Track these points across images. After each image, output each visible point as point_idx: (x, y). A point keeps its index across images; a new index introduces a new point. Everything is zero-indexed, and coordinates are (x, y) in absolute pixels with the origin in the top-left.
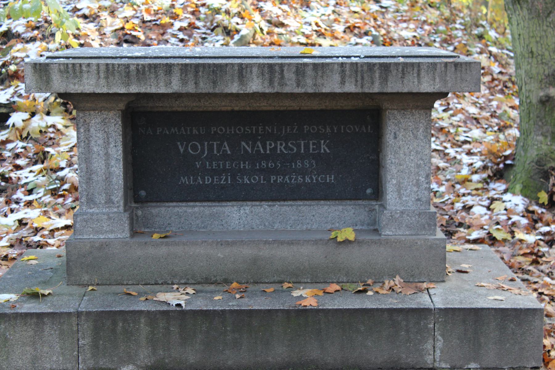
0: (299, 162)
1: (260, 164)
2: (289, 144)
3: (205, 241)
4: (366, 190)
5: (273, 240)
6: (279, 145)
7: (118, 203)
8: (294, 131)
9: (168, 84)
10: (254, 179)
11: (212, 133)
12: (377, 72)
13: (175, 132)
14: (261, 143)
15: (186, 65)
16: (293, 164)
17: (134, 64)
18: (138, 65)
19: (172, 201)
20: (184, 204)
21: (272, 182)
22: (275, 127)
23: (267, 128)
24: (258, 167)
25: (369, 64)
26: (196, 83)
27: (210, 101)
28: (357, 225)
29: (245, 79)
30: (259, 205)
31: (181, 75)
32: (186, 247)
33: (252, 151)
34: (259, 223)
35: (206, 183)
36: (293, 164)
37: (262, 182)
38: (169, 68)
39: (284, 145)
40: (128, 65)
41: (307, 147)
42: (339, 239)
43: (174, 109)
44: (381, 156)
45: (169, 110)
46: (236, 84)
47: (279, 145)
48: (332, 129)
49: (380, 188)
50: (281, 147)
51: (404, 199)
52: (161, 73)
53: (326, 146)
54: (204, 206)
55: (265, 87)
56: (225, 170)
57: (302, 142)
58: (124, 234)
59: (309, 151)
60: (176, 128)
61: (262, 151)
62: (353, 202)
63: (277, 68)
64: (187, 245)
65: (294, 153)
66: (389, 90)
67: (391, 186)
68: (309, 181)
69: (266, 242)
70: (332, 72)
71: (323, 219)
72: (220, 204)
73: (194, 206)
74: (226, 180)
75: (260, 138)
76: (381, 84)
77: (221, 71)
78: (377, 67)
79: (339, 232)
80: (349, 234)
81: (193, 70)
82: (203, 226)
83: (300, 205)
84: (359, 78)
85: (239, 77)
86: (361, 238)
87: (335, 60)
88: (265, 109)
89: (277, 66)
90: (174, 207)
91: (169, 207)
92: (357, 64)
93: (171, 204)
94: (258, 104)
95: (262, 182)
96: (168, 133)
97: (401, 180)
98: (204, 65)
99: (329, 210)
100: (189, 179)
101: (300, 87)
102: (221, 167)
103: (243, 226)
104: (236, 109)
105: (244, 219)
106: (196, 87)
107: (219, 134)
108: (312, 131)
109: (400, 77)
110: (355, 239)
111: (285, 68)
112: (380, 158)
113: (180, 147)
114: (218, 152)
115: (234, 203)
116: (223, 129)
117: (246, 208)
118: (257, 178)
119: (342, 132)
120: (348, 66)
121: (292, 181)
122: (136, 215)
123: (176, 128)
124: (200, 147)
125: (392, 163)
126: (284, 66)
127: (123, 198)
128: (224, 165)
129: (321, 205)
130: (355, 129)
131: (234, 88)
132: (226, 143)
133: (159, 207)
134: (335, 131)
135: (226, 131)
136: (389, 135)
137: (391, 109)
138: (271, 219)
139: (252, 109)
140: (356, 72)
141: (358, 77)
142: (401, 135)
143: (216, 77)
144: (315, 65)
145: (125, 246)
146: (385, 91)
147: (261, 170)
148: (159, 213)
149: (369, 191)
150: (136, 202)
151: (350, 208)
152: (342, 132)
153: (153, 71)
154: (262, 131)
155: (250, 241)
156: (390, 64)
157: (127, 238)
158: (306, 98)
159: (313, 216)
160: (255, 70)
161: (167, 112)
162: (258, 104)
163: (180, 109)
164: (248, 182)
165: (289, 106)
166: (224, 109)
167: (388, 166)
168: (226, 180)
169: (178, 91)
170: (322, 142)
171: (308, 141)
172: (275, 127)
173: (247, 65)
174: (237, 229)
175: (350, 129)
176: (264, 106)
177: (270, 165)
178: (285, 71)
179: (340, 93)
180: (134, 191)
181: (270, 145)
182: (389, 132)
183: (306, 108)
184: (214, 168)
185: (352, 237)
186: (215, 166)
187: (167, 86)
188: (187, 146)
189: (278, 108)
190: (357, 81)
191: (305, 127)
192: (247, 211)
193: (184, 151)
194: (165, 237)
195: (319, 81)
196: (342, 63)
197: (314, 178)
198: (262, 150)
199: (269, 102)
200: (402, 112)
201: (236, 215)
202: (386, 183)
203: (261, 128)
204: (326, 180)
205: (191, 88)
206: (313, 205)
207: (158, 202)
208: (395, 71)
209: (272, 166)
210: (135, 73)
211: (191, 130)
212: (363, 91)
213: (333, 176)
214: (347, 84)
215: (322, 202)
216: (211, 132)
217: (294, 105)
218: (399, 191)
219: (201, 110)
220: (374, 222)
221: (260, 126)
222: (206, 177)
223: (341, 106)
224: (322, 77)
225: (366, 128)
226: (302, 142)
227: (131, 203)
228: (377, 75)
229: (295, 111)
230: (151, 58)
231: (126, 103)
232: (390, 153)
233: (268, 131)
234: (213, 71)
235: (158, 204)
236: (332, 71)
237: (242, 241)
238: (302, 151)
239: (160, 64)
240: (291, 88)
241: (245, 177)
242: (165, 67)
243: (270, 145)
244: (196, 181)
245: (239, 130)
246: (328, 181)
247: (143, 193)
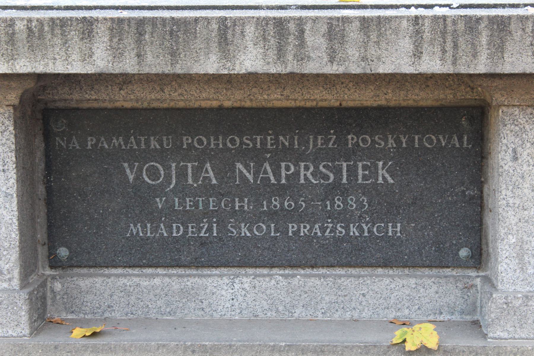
1: (270, 202)
2: (321, 168)
3: (164, 346)
4: (459, 250)
5: (286, 345)
6: (302, 169)
7: (9, 273)
8: (330, 146)
9: (88, 56)
10: (259, 229)
13: (120, 145)
14: (271, 165)
15: (120, 21)
16: (328, 203)
17: (22, 19)
18: (30, 20)
19: (115, 267)
20: (136, 271)
21: (290, 234)
22: (296, 137)
23: (281, 138)
24: (265, 208)
25: (468, 19)
26: (139, 56)
27: (180, 91)
28: (441, 313)
29: (231, 48)
31: (111, 40)
33: (255, 179)
34: (266, 307)
35: (174, 235)
36: (328, 203)
37: (272, 234)
38: (88, 27)
39: (312, 169)
40: (12, 20)
41: (352, 172)
42: (410, 346)
43: (118, 104)
44: (485, 190)
46: (213, 58)
47: (302, 169)
48: (398, 141)
50: (306, 173)
52: (74, 35)
53: (387, 171)
54: (170, 276)
55: (268, 63)
56: (207, 214)
57: (345, 165)
58: (19, 330)
60: (121, 139)
61: (273, 181)
62: (435, 271)
63: (292, 26)
64: (131, 351)
65: (329, 184)
66: (507, 69)
67: (507, 247)
68: (357, 234)
70: (397, 34)
71: (381, 301)
72: (199, 272)
73: (153, 276)
74: (209, 230)
75: (268, 156)
76: (491, 56)
77: (186, 32)
78: (483, 25)
81: (133, 29)
82: (168, 310)
83: (340, 276)
84: (449, 45)
85: (220, 43)
87: (403, 12)
89: (292, 22)
90: (118, 276)
91: (109, 276)
92: (444, 18)
93: (114, 271)
94: (266, 97)
95: (272, 234)
96: (106, 146)
98: (153, 21)
99: (393, 286)
100: (144, 227)
101: (335, 63)
102: (201, 208)
103: (239, 311)
104: (227, 104)
105: (241, 299)
106: (139, 63)
107: (196, 149)
108: (361, 144)
109: (528, 43)
110: (439, 347)
111: (308, 27)
112: (485, 194)
113: (128, 171)
114: (195, 180)
115: (225, 270)
116: (204, 139)
117: (245, 280)
118: (264, 227)
120: (427, 22)
121: (327, 234)
122: (53, 291)
123: (121, 139)
124: (162, 173)
125: (508, 205)
126: (306, 23)
128: (206, 204)
129: (377, 276)
130: (438, 140)
131: (211, 65)
132: (208, 165)
133: (91, 276)
134: (404, 145)
135: (209, 143)
136: (503, 153)
137: (508, 106)
138: (288, 300)
139: (254, 105)
140: (444, 33)
141: (448, 44)
142: (525, 153)
143: (177, 42)
144: (363, 20)
147: (272, 215)
149: (464, 253)
150: (52, 267)
151: (429, 282)
153: (58, 31)
154: (272, 145)
155: (244, 346)
156: (510, 17)
157: (25, 336)
158: (351, 85)
159: (364, 295)
160: (250, 30)
161: (106, 109)
162: (266, 97)
163: (128, 105)
164: (248, 235)
165: (322, 100)
166: (205, 104)
167: (500, 210)
168: (209, 230)
169: (106, 71)
170: (381, 164)
171: (355, 162)
172: (296, 137)
173: (235, 21)
174: (228, 316)
175: (430, 141)
176: (276, 99)
177: (286, 204)
179: (412, 76)
180: (49, 249)
181: (288, 169)
182: (504, 148)
183: (351, 104)
184: (188, 208)
186: (190, 206)
187: (85, 60)
188: (140, 169)
189: (302, 104)
190: (444, 51)
191: (350, 137)
192: (246, 286)
194: (94, 334)
195: (373, 51)
196: (416, 17)
197: (366, 228)
198: (272, 178)
199: (285, 93)
201: (226, 293)
202: (496, 241)
203: (271, 139)
204: (387, 233)
205: (129, 65)
206: (363, 276)
207: (91, 267)
208: (520, 32)
209: (290, 206)
210: (25, 36)
211: (147, 143)
212: (456, 71)
213: (399, 225)
214: (425, 57)
215: (380, 271)
216: (182, 144)
217: (329, 97)
218: (520, 257)
219: (165, 105)
221: (270, 135)
222: (174, 225)
223: (414, 100)
224: (377, 43)
225: (460, 139)
226: (345, 165)
227: (44, 268)
228: (484, 40)
229: (331, 109)
230: (59, 8)
231: (20, 92)
232: (504, 186)
233: (283, 143)
234: (171, 33)
235: (92, 270)
236: (396, 31)
237: (230, 346)
238: (344, 181)
239: (71, 19)
240: (318, 65)
241: (243, 225)
243: (288, 169)
244: (156, 231)
245: (233, 141)
246: (390, 234)
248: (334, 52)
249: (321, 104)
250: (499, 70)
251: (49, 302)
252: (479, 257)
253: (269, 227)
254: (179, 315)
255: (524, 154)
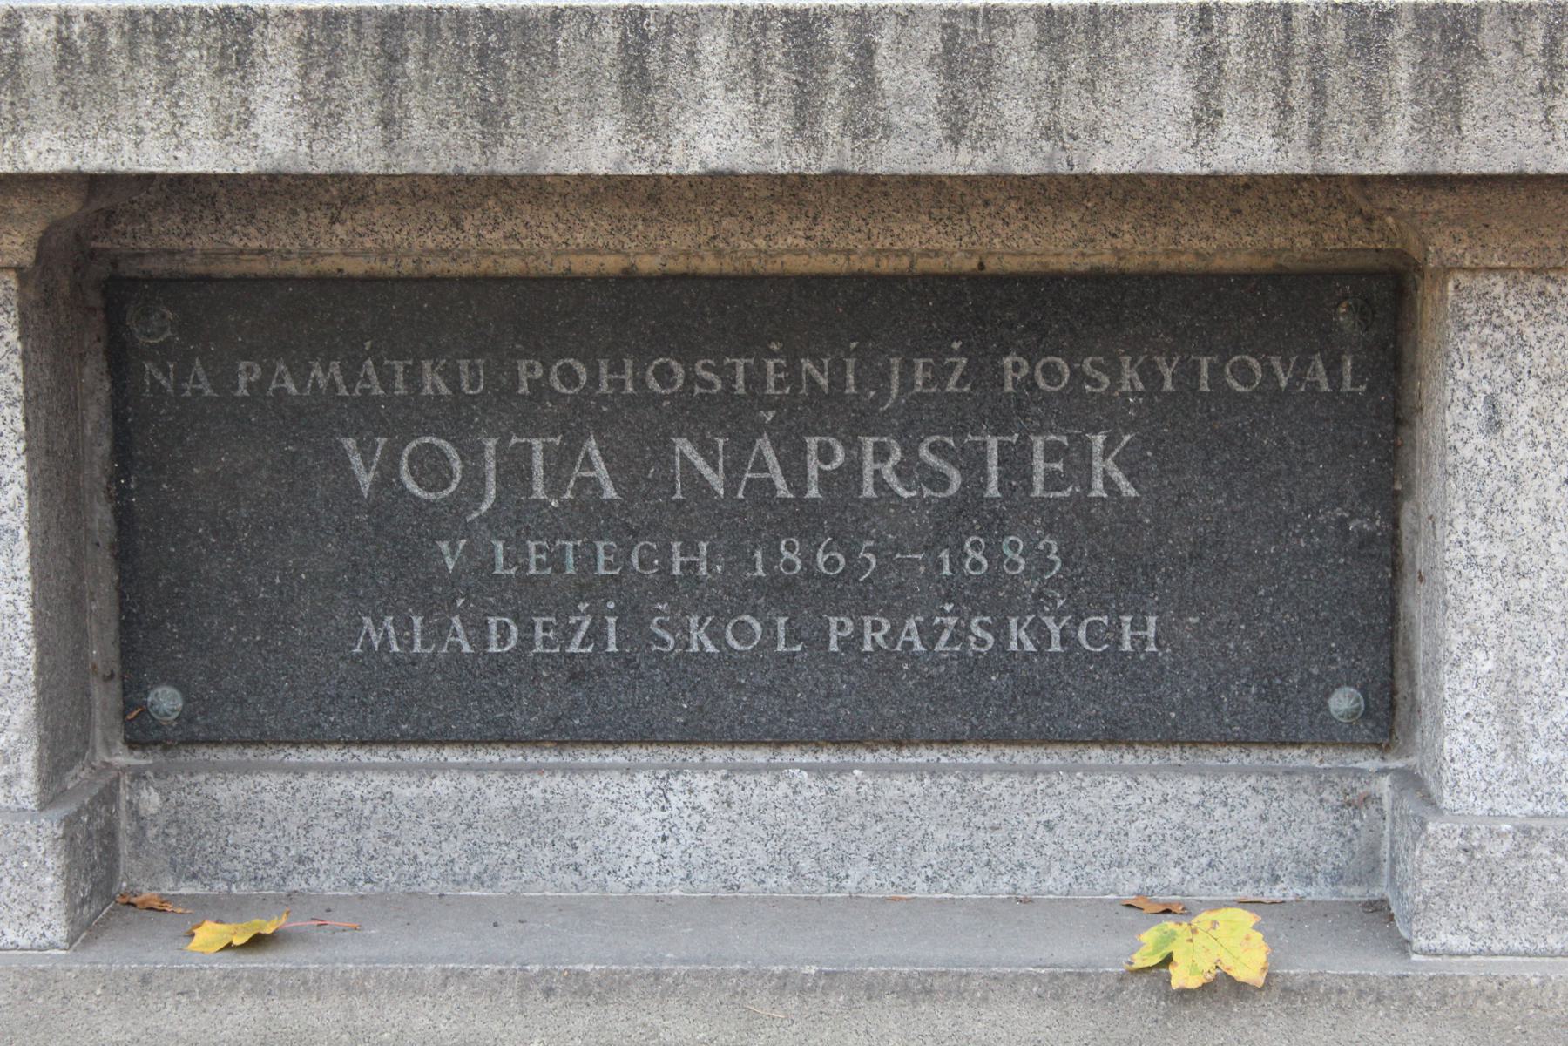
0: (975, 546)
1: (773, 554)
2: (924, 452)
3: (463, 974)
4: (1328, 695)
6: (869, 458)
8: (951, 387)
9: (237, 122)
10: (741, 631)
11: (524, 389)
12: (1403, 57)
13: (332, 384)
14: (776, 445)
20: (381, 756)
21: (834, 647)
22: (851, 363)
23: (807, 364)
24: (760, 572)
26: (386, 121)
27: (509, 226)
28: (1276, 879)
29: (659, 99)
30: (769, 768)
31: (304, 76)
32: (357, 1001)
33: (731, 484)
34: (763, 861)
35: (493, 649)
37: (781, 648)
39: (896, 456)
41: (1015, 464)
42: (1182, 976)
43: (327, 265)
44: (1407, 517)
45: (301, 269)
46: (607, 128)
47: (869, 458)
48: (1150, 374)
49: (1402, 684)
50: (880, 468)
51: (1538, 755)
52: (195, 60)
53: (1117, 461)
54: (480, 770)
55: (769, 144)
56: (587, 587)
57: (993, 443)
58: (37, 928)
59: (1030, 487)
60: (335, 368)
61: (783, 490)
62: (1257, 756)
64: (365, 991)
66: (1471, 162)
67: (1468, 685)
69: (784, 984)
71: (1101, 843)
72: (567, 758)
73: (429, 770)
74: (596, 634)
76: (1422, 124)
77: (524, 51)
78: (1400, 33)
79: (1182, 930)
80: (1231, 944)
81: (370, 44)
82: (474, 870)
83: (979, 771)
84: (1300, 92)
85: (625, 85)
86: (1298, 969)
88: (797, 265)
91: (300, 771)
93: (315, 755)
94: (761, 243)
95: (781, 648)
96: (293, 389)
97: (1521, 657)
99: (1134, 799)
101: (964, 145)
103: (681, 873)
104: (648, 264)
105: (687, 836)
106: (387, 144)
108: (1042, 384)
109: (1532, 85)
111: (884, 38)
112: (1405, 529)
114: (555, 488)
115: (640, 754)
116: (580, 368)
117: (700, 781)
118: (757, 626)
119: (1205, 388)
121: (941, 646)
122: (135, 814)
124: (457, 466)
125: (1471, 562)
127: (33, 734)
129: (1089, 770)
130: (1269, 371)
131: (598, 148)
132: (592, 445)
133: (247, 769)
134: (1168, 386)
135: (594, 380)
136: (1457, 409)
137: (1473, 270)
138: (826, 840)
139: (728, 267)
140: (1284, 56)
143: (500, 84)
145: (38, 991)
146: (1445, 166)
147: (780, 590)
148: (247, 804)
149: (1342, 702)
150: (132, 744)
151: (1241, 786)
152: (1205, 388)
153: (148, 49)
154: (779, 384)
155: (697, 975)
157: (53, 946)
158: (1011, 208)
159: (1049, 826)
160: (714, 46)
161: (290, 279)
162: (761, 243)
163: (355, 267)
164: (711, 648)
165: (926, 253)
166: (582, 265)
168: (596, 634)
169: (289, 166)
170: (1099, 440)
171: (1024, 437)
172: (851, 363)
175: (1245, 374)
176: (792, 248)
177: (821, 558)
178: (882, 51)
179: (1192, 181)
180: (125, 690)
181: (826, 454)
183: (1012, 264)
184: (533, 571)
185: (1249, 965)
188: (393, 456)
189: (868, 264)
190: (1285, 109)
191: (1008, 361)
192: (704, 799)
193: (375, 485)
194: (258, 942)
195: (1075, 109)
197: (1055, 631)
198: (780, 482)
199: (818, 232)
200: (1535, 283)
201: (644, 821)
202: (1436, 666)
203: (778, 369)
204: (1119, 643)
205: (357, 150)
206: (1046, 771)
207: (247, 743)
208: (1508, 53)
209: (832, 563)
210: (50, 62)
211: (413, 377)
212: (1322, 168)
213: (1152, 620)
214: (1230, 127)
215: (1096, 754)
216: (516, 383)
217: (949, 244)
218: (1508, 713)
219: (466, 269)
220: (1370, 865)
221: (773, 355)
223: (1198, 254)
224: (1090, 84)
225: (1333, 368)
226: (993, 443)
227: (108, 745)
228: (1403, 75)
229: (953, 278)
231: (38, 228)
234: (483, 54)
236: (1144, 51)
237: (657, 976)
238: (993, 490)
240: (913, 149)
241: (694, 620)
242: (215, 32)
243: (826, 454)
245: (664, 375)
247: (166, 700)
248: (962, 110)
249: (923, 265)
250: (1445, 165)
251: (125, 846)
252: (1388, 712)
253: (770, 625)
254: (506, 885)
255: (1521, 414)
